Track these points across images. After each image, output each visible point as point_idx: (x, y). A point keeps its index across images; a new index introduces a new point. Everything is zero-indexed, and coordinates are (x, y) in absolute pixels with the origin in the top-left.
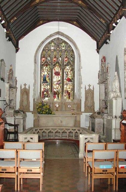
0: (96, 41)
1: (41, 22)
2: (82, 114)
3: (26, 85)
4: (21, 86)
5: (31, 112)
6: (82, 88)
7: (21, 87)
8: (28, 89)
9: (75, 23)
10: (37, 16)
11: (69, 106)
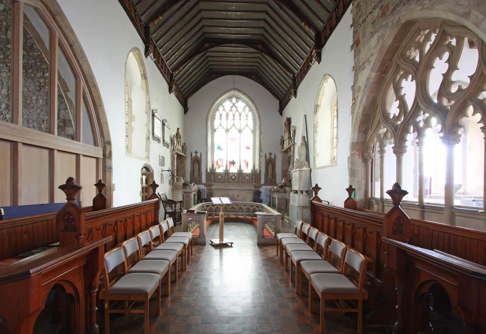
0: (279, 100)
1: (214, 76)
5: (203, 184)
6: (430, 45)
7: (191, 155)
9: (254, 77)
10: (206, 58)
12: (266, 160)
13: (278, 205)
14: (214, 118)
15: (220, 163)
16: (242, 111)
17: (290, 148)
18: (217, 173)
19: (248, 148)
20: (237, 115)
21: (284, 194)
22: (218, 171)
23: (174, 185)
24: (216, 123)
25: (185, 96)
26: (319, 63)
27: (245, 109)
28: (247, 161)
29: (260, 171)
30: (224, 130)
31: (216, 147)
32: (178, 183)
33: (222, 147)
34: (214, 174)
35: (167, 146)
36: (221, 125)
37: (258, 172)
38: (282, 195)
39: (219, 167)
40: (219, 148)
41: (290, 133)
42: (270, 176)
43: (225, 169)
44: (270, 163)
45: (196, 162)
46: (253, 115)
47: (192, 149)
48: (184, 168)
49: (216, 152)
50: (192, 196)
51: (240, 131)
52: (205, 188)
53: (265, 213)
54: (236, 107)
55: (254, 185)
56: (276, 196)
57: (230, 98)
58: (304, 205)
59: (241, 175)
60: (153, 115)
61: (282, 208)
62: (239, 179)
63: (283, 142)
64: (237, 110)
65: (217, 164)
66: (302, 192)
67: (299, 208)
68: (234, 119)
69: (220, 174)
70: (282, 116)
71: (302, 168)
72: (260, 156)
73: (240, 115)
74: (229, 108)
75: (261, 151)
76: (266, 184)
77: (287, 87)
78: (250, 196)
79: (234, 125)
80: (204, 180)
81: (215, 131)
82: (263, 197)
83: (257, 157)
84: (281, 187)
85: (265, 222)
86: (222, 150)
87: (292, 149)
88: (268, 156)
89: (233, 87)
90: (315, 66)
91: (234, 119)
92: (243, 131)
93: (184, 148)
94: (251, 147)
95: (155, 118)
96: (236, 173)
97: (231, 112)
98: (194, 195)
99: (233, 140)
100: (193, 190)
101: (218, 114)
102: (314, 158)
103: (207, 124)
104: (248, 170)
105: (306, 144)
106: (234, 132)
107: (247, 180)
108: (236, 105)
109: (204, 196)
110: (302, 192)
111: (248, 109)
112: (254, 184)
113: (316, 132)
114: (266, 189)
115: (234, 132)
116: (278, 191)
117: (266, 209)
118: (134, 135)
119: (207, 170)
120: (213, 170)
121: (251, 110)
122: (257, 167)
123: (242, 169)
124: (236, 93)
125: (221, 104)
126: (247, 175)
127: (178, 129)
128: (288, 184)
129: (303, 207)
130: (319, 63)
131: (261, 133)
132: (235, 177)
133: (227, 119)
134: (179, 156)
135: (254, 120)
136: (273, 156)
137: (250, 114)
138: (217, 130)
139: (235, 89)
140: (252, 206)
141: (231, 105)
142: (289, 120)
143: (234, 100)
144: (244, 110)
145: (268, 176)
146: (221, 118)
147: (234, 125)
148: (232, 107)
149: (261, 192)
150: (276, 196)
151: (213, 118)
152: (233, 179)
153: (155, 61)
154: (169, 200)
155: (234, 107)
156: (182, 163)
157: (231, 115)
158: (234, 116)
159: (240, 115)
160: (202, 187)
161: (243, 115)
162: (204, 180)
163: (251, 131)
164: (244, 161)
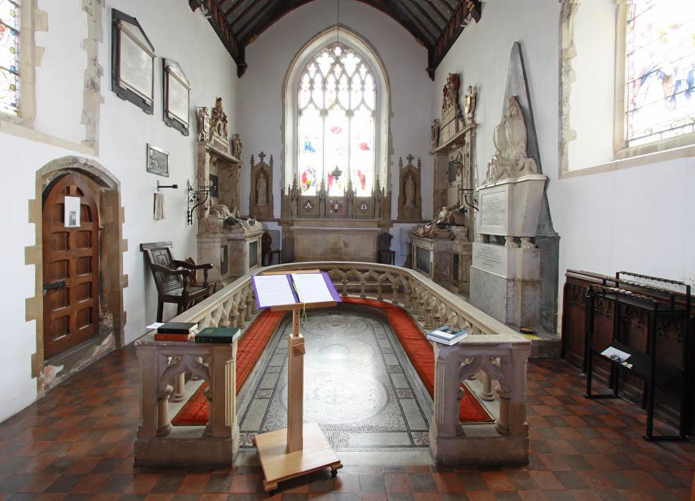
2: (392, 227)
3: (264, 156)
4: (401, 160)
8: (269, 165)
11: (364, 207)
12: (401, 169)
13: (436, 267)
14: (299, 88)
15: (309, 177)
16: (354, 73)
17: (460, 141)
18: (304, 197)
20: (344, 80)
21: (449, 242)
25: (239, 38)
26: (477, 22)
27: (360, 70)
28: (363, 173)
29: (390, 193)
30: (319, 112)
31: (301, 146)
32: (213, 220)
33: (313, 146)
34: (297, 200)
35: (183, 129)
36: (311, 101)
37: (385, 195)
38: (444, 245)
39: (308, 186)
40: (308, 147)
41: (458, 107)
42: (409, 203)
43: (319, 189)
44: (410, 177)
45: (262, 175)
46: (376, 81)
47: (255, 147)
48: (236, 187)
50: (247, 247)
51: (350, 113)
52: (280, 228)
53: (464, 338)
54: (342, 65)
55: (378, 222)
56: (429, 245)
57: (330, 47)
58: (527, 278)
60: (166, 70)
61: (444, 273)
62: (347, 209)
63: (437, 132)
64: (344, 72)
65: (304, 180)
66: (517, 240)
67: (511, 284)
68: (337, 89)
69: (309, 200)
70: (433, 79)
71: (517, 177)
72: (390, 163)
73: (350, 81)
75: (391, 151)
76: (401, 219)
77: (451, 9)
78: (370, 248)
79: (337, 101)
80: (277, 213)
81: (300, 113)
82: (395, 246)
83: (384, 164)
84: (442, 226)
85: (468, 372)
86: (314, 151)
87: (467, 139)
88: (406, 163)
89: (336, 22)
90: (471, 27)
91: (337, 89)
92: (356, 113)
93: (235, 145)
94: (371, 146)
95: (170, 76)
96: (341, 198)
97: (331, 76)
98: (253, 245)
99: (335, 130)
100: (247, 234)
102: (562, 147)
103: (283, 97)
104: (364, 192)
105: (522, 111)
106: (337, 116)
108: (343, 61)
109: (278, 245)
110: (517, 240)
111: (366, 70)
112: (377, 219)
113: (567, 72)
114: (401, 230)
115: (337, 116)
116: (435, 236)
117: (462, 317)
118: (45, 73)
119: (283, 192)
120: (295, 191)
121: (371, 71)
122: (383, 185)
123: (354, 189)
124: (344, 36)
125: (311, 59)
127: (219, 100)
128: (457, 219)
129: (524, 282)
130: (477, 22)
131: (391, 115)
132: (340, 206)
133: (324, 88)
134: (220, 161)
135: (377, 91)
136: (415, 163)
137: (369, 80)
138: (304, 112)
139: (340, 26)
141: (333, 61)
142: (456, 80)
143: (338, 51)
144: (357, 71)
146: (311, 88)
147: (337, 101)
148: (333, 65)
149: (392, 237)
150: (429, 245)
151: (297, 88)
152: (336, 211)
153: (209, 19)
154: (178, 263)
155: (338, 65)
156: (231, 176)
157: (331, 80)
158: (337, 82)
159: (350, 81)
160: (273, 226)
161: (356, 80)
163: (370, 113)
164: (356, 173)
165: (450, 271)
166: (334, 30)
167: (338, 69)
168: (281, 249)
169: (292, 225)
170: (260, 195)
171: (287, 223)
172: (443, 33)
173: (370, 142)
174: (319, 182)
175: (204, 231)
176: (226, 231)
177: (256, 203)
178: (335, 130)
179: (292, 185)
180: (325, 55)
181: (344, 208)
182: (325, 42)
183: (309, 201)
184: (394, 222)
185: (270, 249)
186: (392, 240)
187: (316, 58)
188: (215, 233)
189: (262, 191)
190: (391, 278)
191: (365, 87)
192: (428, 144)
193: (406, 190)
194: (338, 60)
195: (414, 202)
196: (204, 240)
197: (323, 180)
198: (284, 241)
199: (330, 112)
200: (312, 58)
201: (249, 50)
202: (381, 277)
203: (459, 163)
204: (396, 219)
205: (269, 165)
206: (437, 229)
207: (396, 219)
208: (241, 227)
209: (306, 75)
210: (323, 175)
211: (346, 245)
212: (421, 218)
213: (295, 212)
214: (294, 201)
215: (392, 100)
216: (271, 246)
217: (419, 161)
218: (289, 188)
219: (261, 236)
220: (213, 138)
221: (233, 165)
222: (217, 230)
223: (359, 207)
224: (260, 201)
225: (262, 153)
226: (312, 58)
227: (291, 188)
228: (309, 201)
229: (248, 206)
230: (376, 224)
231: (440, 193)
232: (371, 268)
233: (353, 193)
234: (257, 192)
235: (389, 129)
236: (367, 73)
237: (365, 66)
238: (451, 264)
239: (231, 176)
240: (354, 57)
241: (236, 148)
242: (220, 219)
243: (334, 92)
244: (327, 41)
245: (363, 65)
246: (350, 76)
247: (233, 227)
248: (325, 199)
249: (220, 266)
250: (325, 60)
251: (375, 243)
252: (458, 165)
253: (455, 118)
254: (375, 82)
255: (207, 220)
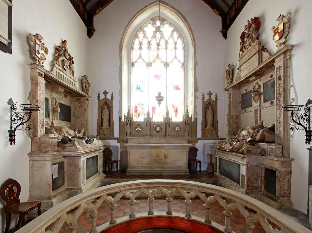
2: (198, 143)
3: (107, 93)
4: (203, 96)
8: (111, 100)
11: (178, 129)
12: (204, 102)
13: (248, 180)
14: (132, 48)
15: (140, 109)
19: (177, 88)
20: (162, 43)
21: (260, 158)
22: (135, 119)
23: (37, 142)
24: (135, 55)
29: (196, 119)
30: (146, 64)
31: (134, 88)
34: (130, 124)
36: (140, 57)
37: (193, 120)
39: (139, 115)
40: (138, 89)
42: (209, 126)
43: (146, 116)
44: (210, 107)
45: (106, 107)
48: (84, 114)
49: (135, 95)
50: (83, 162)
51: (166, 65)
52: (118, 144)
54: (161, 32)
55: (188, 139)
59: (169, 125)
61: (256, 185)
63: (230, 73)
65: (136, 111)
69: (139, 124)
70: (226, 38)
72: (196, 98)
73: (167, 43)
74: (152, 34)
75: (196, 89)
76: (204, 137)
80: (116, 134)
81: (133, 65)
83: (191, 99)
86: (142, 91)
88: (207, 98)
91: (158, 49)
93: (84, 82)
94: (182, 87)
97: (154, 40)
99: (157, 77)
101: (137, 42)
103: (120, 51)
104: (178, 118)
106: (158, 67)
107: (177, 132)
112: (187, 138)
114: (204, 145)
115: (158, 67)
119: (120, 119)
120: (129, 118)
121: (181, 36)
122: (191, 113)
123: (170, 116)
125: (140, 28)
126: (177, 125)
128: (268, 137)
131: (196, 64)
132: (161, 128)
133: (149, 48)
135: (185, 49)
136: (213, 98)
137: (180, 42)
138: (135, 65)
140: (208, 195)
141: (154, 29)
144: (172, 36)
145: (206, 126)
146: (141, 48)
148: (155, 32)
149: (197, 150)
152: (158, 132)
155: (158, 33)
157: (154, 43)
160: (113, 143)
161: (171, 43)
162: (116, 134)
163: (180, 65)
164: (171, 106)
165: (261, 182)
166: (156, 5)
167: (158, 35)
168: (119, 159)
169: (127, 142)
170: (104, 120)
171: (124, 141)
172: (230, 8)
173: (180, 84)
174: (146, 112)
175: (37, 149)
176: (60, 149)
177: (102, 126)
178: (157, 77)
179: (126, 113)
180: (150, 26)
181: (163, 130)
182: (149, 16)
183: (138, 125)
184: (199, 139)
185: (111, 160)
186: (198, 152)
187: (144, 28)
188: (46, 152)
189: (106, 119)
190: (222, 203)
191: (177, 47)
192: (225, 83)
193: (207, 116)
194: (158, 29)
195: (213, 125)
196: (35, 158)
197: (149, 110)
198: (121, 154)
199: (153, 64)
200: (141, 27)
201: (96, 19)
202: (209, 199)
203: (257, 91)
204: (200, 137)
205: (111, 100)
206: (249, 146)
207: (200, 137)
208: (74, 145)
209: (137, 39)
210: (149, 106)
211: (166, 157)
212: (218, 136)
213: (129, 133)
214: (128, 125)
215: (197, 53)
216: (112, 157)
217: (216, 96)
218: (125, 116)
219: (102, 151)
220: (55, 69)
221: (82, 98)
222: (49, 149)
223: (174, 129)
224: (104, 125)
225: (106, 91)
226: (141, 27)
227: (126, 116)
228: (138, 125)
229: (96, 129)
230: (187, 141)
231: (234, 117)
232: (197, 189)
233: (170, 119)
234: (102, 119)
235: (195, 74)
236: (178, 37)
237: (177, 32)
238: (262, 177)
239: (81, 106)
240: (169, 26)
241: (84, 86)
242: (55, 137)
243: (156, 51)
244: (152, 14)
245: (175, 32)
246: (167, 40)
247: (67, 145)
248: (150, 124)
249: (51, 182)
250: (149, 29)
251: (187, 155)
252: (256, 93)
253: (258, 52)
254: (184, 43)
255: (40, 139)
